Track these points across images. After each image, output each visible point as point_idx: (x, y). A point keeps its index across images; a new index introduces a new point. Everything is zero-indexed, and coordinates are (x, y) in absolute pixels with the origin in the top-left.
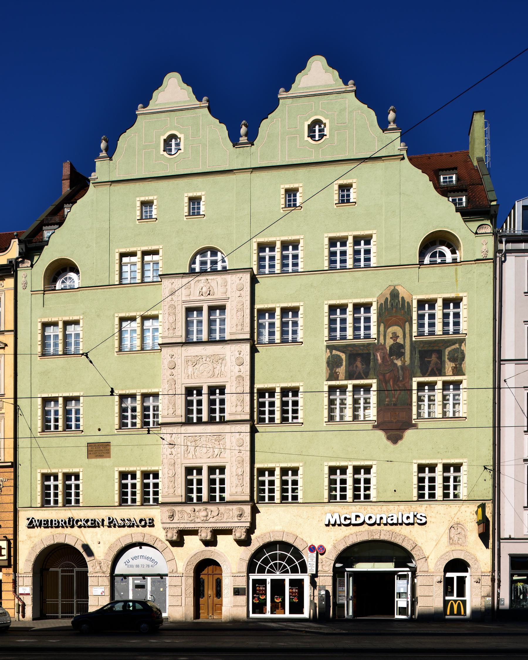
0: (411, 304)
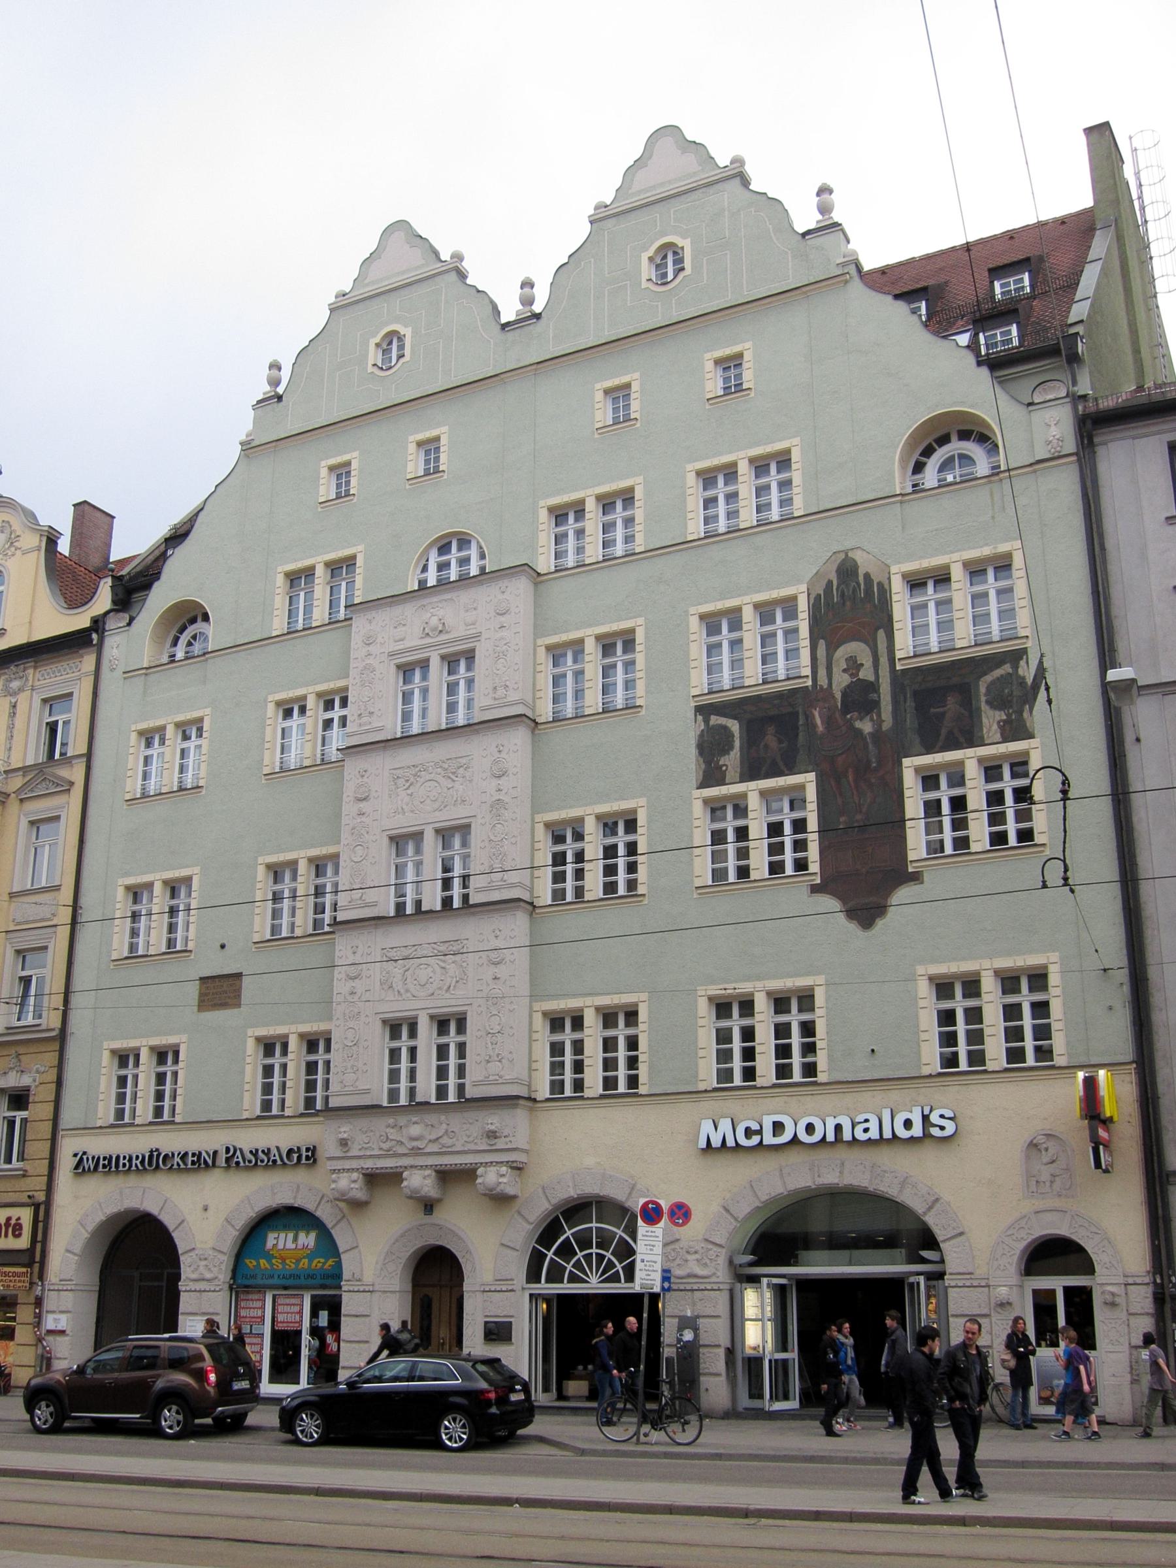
0: (887, 587)
